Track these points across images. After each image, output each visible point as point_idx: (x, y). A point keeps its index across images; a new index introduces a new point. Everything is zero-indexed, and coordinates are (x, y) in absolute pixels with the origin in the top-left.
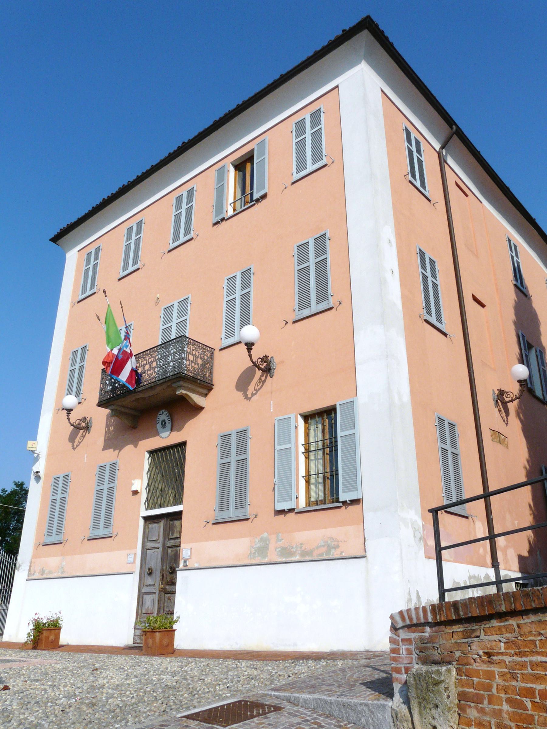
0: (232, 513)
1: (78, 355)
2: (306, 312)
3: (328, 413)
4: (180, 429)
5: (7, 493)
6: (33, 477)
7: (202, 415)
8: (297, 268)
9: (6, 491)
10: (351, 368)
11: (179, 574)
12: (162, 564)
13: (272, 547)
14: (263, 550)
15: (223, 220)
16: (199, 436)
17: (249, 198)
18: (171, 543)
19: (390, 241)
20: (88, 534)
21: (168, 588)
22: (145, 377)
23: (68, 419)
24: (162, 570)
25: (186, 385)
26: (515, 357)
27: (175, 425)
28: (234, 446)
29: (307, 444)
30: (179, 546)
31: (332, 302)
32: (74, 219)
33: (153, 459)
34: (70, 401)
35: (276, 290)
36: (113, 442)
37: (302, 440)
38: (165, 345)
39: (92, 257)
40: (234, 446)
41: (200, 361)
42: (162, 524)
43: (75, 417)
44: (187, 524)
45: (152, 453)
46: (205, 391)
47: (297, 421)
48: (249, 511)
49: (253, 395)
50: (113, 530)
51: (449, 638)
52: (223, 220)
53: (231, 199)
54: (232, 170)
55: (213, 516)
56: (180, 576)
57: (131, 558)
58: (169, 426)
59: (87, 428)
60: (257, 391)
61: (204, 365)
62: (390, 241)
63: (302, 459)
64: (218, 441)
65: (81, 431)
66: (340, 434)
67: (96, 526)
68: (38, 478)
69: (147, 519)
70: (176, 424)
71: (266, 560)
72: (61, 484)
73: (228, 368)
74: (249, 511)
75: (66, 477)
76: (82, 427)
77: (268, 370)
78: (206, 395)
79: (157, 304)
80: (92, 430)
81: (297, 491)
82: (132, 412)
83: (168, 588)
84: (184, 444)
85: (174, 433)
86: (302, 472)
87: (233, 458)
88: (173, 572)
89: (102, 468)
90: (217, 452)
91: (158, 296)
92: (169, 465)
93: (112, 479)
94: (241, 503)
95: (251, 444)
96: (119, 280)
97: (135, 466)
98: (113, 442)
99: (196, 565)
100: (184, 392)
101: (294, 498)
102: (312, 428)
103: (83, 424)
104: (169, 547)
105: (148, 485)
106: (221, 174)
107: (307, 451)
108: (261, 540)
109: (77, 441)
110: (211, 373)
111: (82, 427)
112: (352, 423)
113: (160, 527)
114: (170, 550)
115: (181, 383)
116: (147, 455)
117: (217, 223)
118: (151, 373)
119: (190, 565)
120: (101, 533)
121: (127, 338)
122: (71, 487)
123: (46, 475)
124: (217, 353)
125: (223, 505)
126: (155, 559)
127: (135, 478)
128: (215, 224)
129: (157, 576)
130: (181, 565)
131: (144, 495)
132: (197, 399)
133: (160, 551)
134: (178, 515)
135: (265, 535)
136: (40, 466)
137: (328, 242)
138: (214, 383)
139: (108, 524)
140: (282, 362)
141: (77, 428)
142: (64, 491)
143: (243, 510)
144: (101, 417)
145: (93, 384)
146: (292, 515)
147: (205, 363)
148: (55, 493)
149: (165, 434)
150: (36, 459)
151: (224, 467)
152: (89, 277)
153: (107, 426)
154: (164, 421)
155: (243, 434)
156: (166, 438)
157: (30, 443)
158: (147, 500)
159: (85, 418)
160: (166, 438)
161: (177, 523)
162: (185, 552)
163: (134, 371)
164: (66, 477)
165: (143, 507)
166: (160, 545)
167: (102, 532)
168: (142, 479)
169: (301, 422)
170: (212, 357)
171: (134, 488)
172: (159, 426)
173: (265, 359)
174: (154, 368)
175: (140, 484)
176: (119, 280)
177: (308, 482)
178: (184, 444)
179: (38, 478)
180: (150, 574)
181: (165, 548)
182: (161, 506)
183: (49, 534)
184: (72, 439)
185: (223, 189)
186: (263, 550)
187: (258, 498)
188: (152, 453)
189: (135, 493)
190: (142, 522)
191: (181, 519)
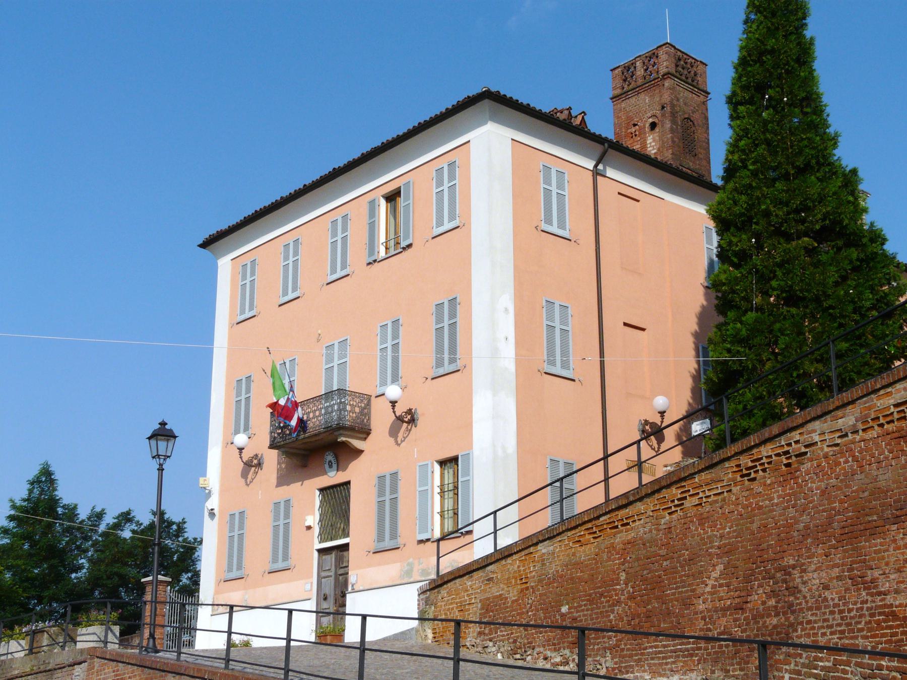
0: (387, 544)
1: (242, 386)
2: (441, 371)
3: (454, 460)
4: (344, 470)
5: (142, 527)
6: (206, 514)
7: (363, 457)
8: (435, 327)
9: (141, 524)
10: (468, 426)
11: (348, 596)
12: (335, 590)
13: (415, 570)
14: (409, 573)
15: (375, 261)
16: (360, 475)
17: (399, 246)
18: (341, 571)
19: (506, 310)
20: (268, 569)
21: (341, 609)
22: (310, 424)
23: (241, 458)
24: (335, 594)
25: (345, 433)
26: (688, 375)
27: (340, 466)
28: (388, 484)
29: (442, 486)
30: (347, 573)
31: (459, 364)
32: (224, 226)
33: (323, 496)
34: (241, 439)
35: (418, 351)
36: (283, 480)
37: (437, 482)
38: (328, 395)
39: (247, 270)
40: (388, 484)
41: (357, 410)
42: (333, 555)
43: (246, 456)
44: (353, 554)
45: (322, 490)
46: (364, 436)
47: (433, 467)
48: (400, 541)
49: (402, 441)
50: (291, 563)
51: (432, 595)
52: (375, 261)
53: (383, 239)
54: (383, 202)
55: (373, 546)
56: (349, 597)
57: (308, 587)
58: (335, 466)
59: (259, 465)
60: (405, 438)
61: (361, 412)
62: (506, 310)
63: (437, 498)
64: (375, 481)
65: (253, 469)
66: (460, 479)
67: (275, 560)
68: (212, 514)
69: (321, 551)
70: (341, 464)
71: (412, 580)
72: (236, 522)
73: (381, 419)
74: (400, 541)
75: (242, 513)
76: (253, 465)
77: (413, 421)
78: (365, 439)
79: (318, 340)
80: (264, 466)
81: (433, 524)
82: (303, 452)
83: (341, 609)
84: (348, 483)
85: (340, 473)
86: (437, 508)
87: (387, 497)
88: (344, 596)
89: (277, 504)
90: (375, 491)
91: (319, 332)
92: (337, 500)
93: (287, 515)
94: (394, 535)
95: (401, 484)
96: (280, 306)
97: (306, 499)
98: (283, 480)
99: (361, 588)
100: (344, 439)
101: (430, 530)
102: (446, 472)
103: (255, 462)
104: (341, 575)
105: (320, 521)
106: (373, 205)
107: (442, 492)
108: (408, 564)
109: (250, 476)
110: (369, 419)
111: (253, 465)
112: (467, 472)
113: (331, 558)
114: (341, 578)
115: (341, 432)
116: (318, 493)
117: (369, 264)
118: (316, 421)
119: (356, 588)
120: (280, 566)
121: (292, 389)
122: (247, 523)
123: (220, 511)
124: (373, 399)
125: (380, 537)
126: (329, 587)
127: (308, 515)
128: (369, 264)
129: (331, 600)
130: (350, 589)
131: (316, 530)
132: (357, 443)
133: (332, 579)
134: (345, 547)
135: (411, 560)
136: (213, 503)
137: (458, 306)
138: (372, 427)
139: (286, 557)
140: (423, 414)
141: (248, 465)
142: (241, 527)
143: (395, 541)
144: (272, 458)
145: (262, 422)
146: (429, 543)
147: (363, 409)
148: (232, 529)
149: (332, 474)
150: (209, 495)
151: (381, 504)
152: (246, 294)
153: (279, 463)
154: (330, 461)
155: (394, 475)
156: (333, 478)
157: (201, 480)
158: (320, 534)
159: (256, 455)
160: (333, 478)
161: (345, 553)
162: (352, 579)
163: (301, 421)
164: (242, 513)
165: (316, 541)
166: (332, 573)
167: (280, 565)
168: (314, 514)
169: (437, 467)
170: (369, 404)
171: (307, 524)
172: (327, 466)
173: (409, 412)
174: (317, 417)
175: (313, 519)
176: (280, 306)
177: (442, 516)
178: (348, 483)
179: (212, 514)
180: (325, 599)
181: (337, 576)
182: (331, 540)
183: (230, 569)
184: (244, 475)
185: (374, 226)
186: (409, 573)
187: (409, 531)
188: (322, 490)
189: (309, 528)
190: (316, 554)
191: (348, 550)
